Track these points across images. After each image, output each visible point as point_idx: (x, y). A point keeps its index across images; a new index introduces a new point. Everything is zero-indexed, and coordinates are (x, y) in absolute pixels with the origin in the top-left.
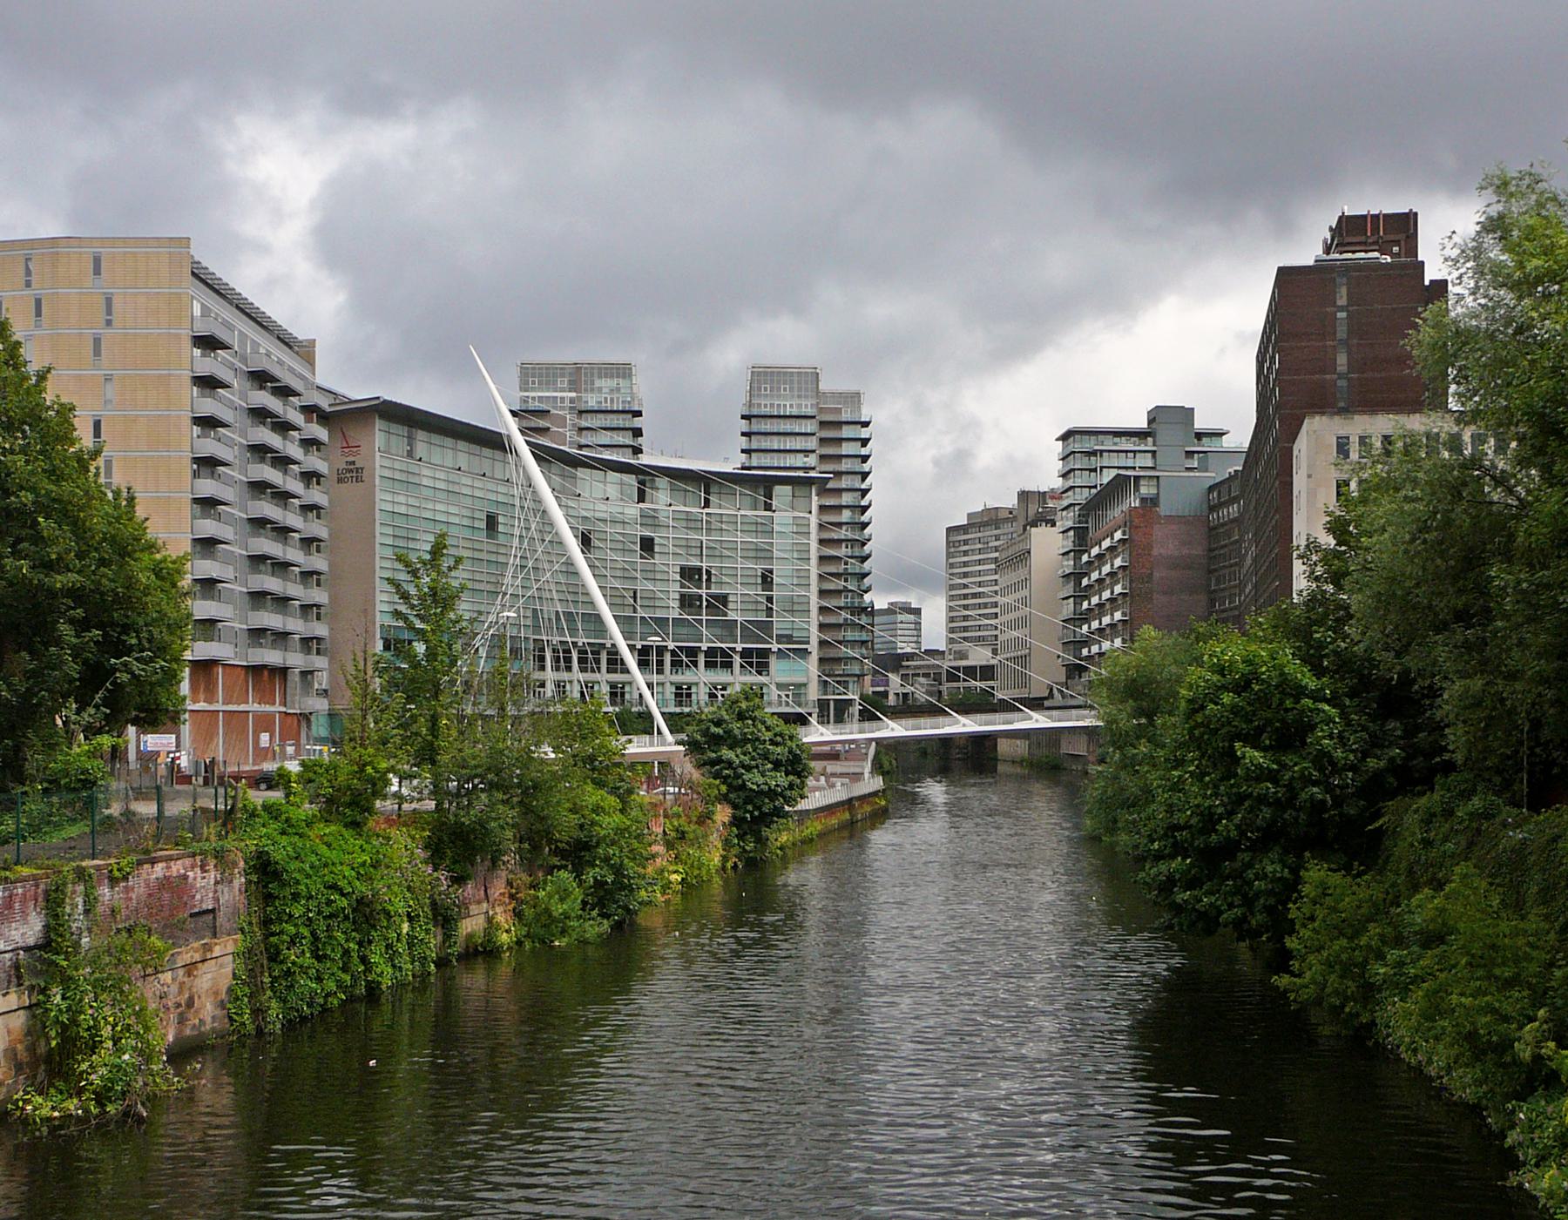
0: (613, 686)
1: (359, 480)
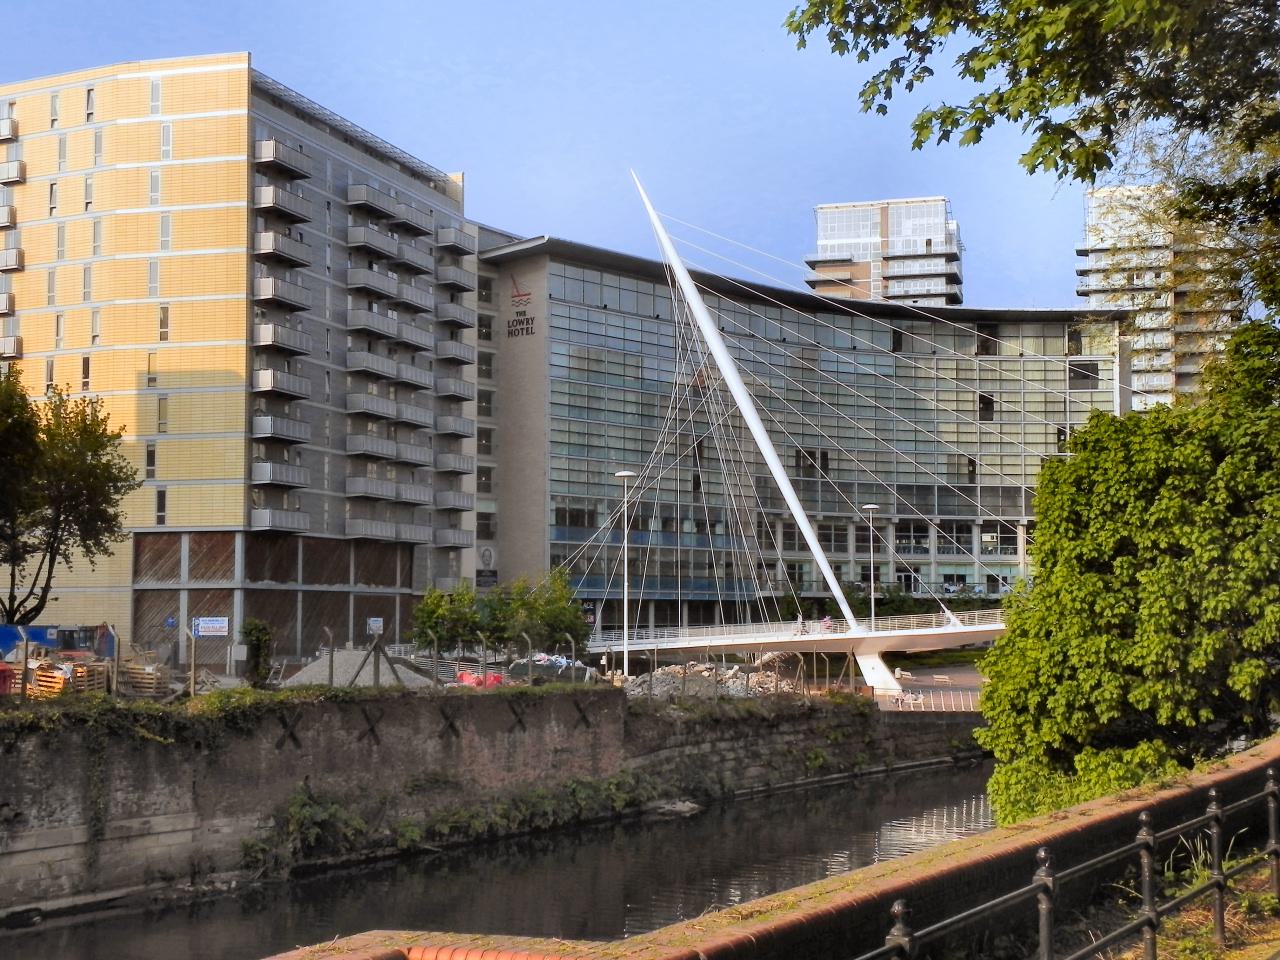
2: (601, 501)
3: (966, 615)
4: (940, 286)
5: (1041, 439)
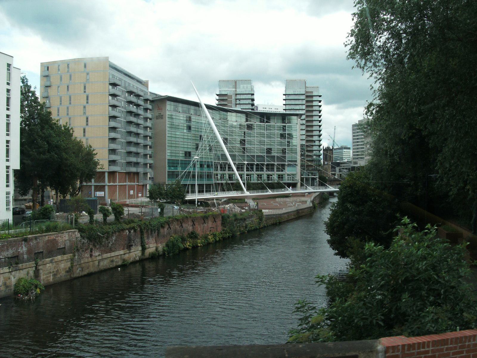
0: (229, 175)
1: (162, 118)
3: (272, 190)
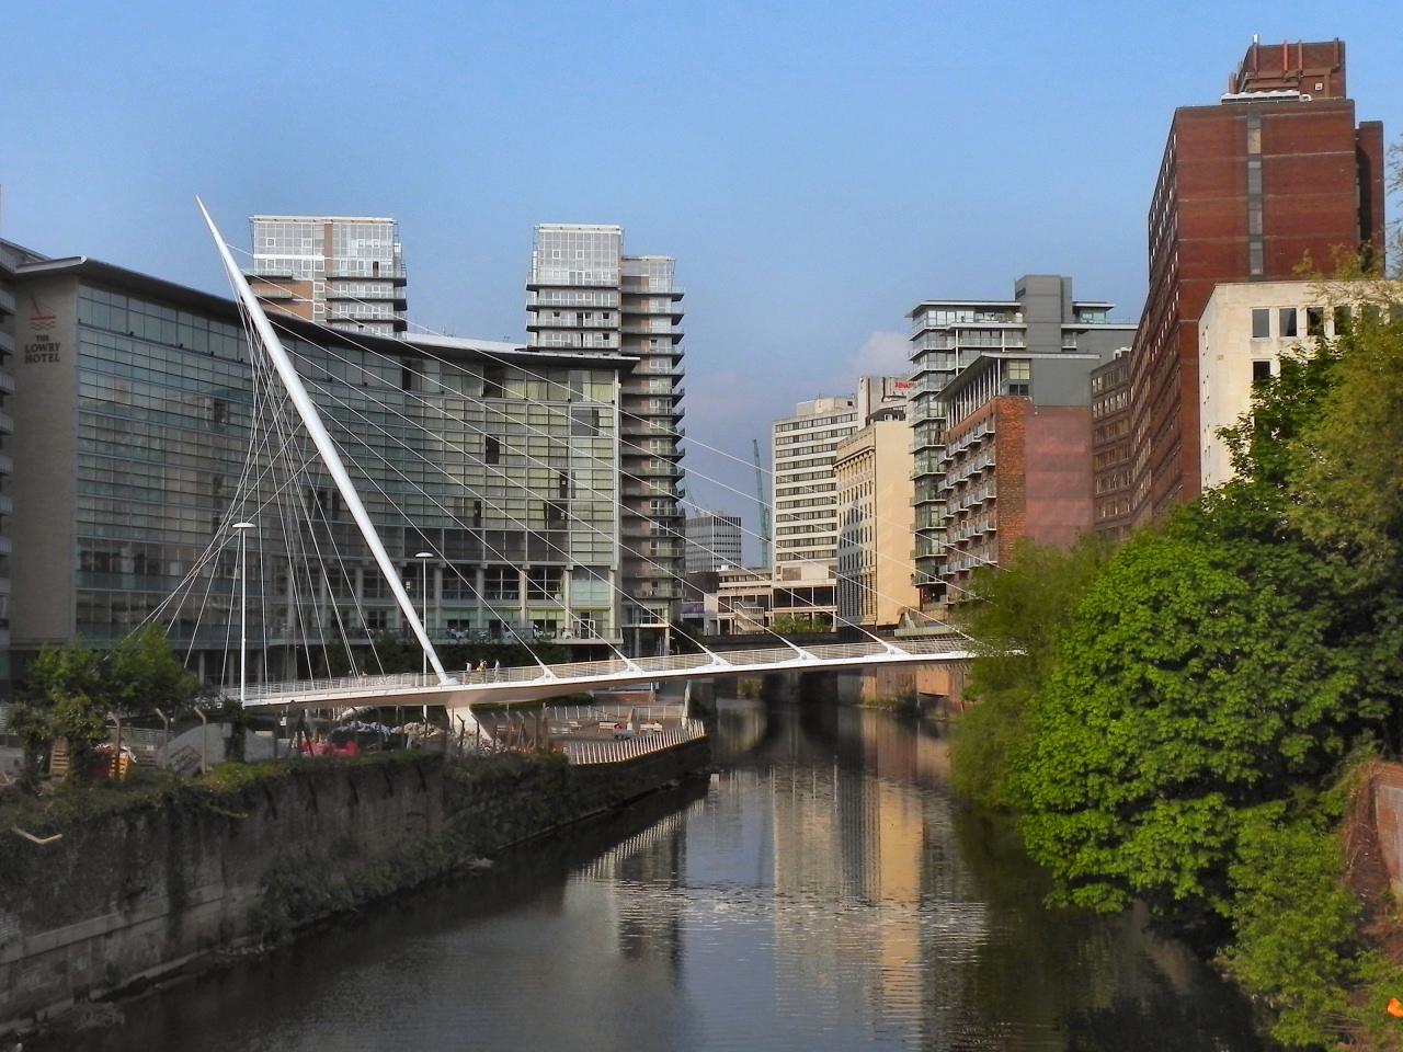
0: (372, 613)
2: (125, 544)
4: (386, 312)
5: (544, 484)
